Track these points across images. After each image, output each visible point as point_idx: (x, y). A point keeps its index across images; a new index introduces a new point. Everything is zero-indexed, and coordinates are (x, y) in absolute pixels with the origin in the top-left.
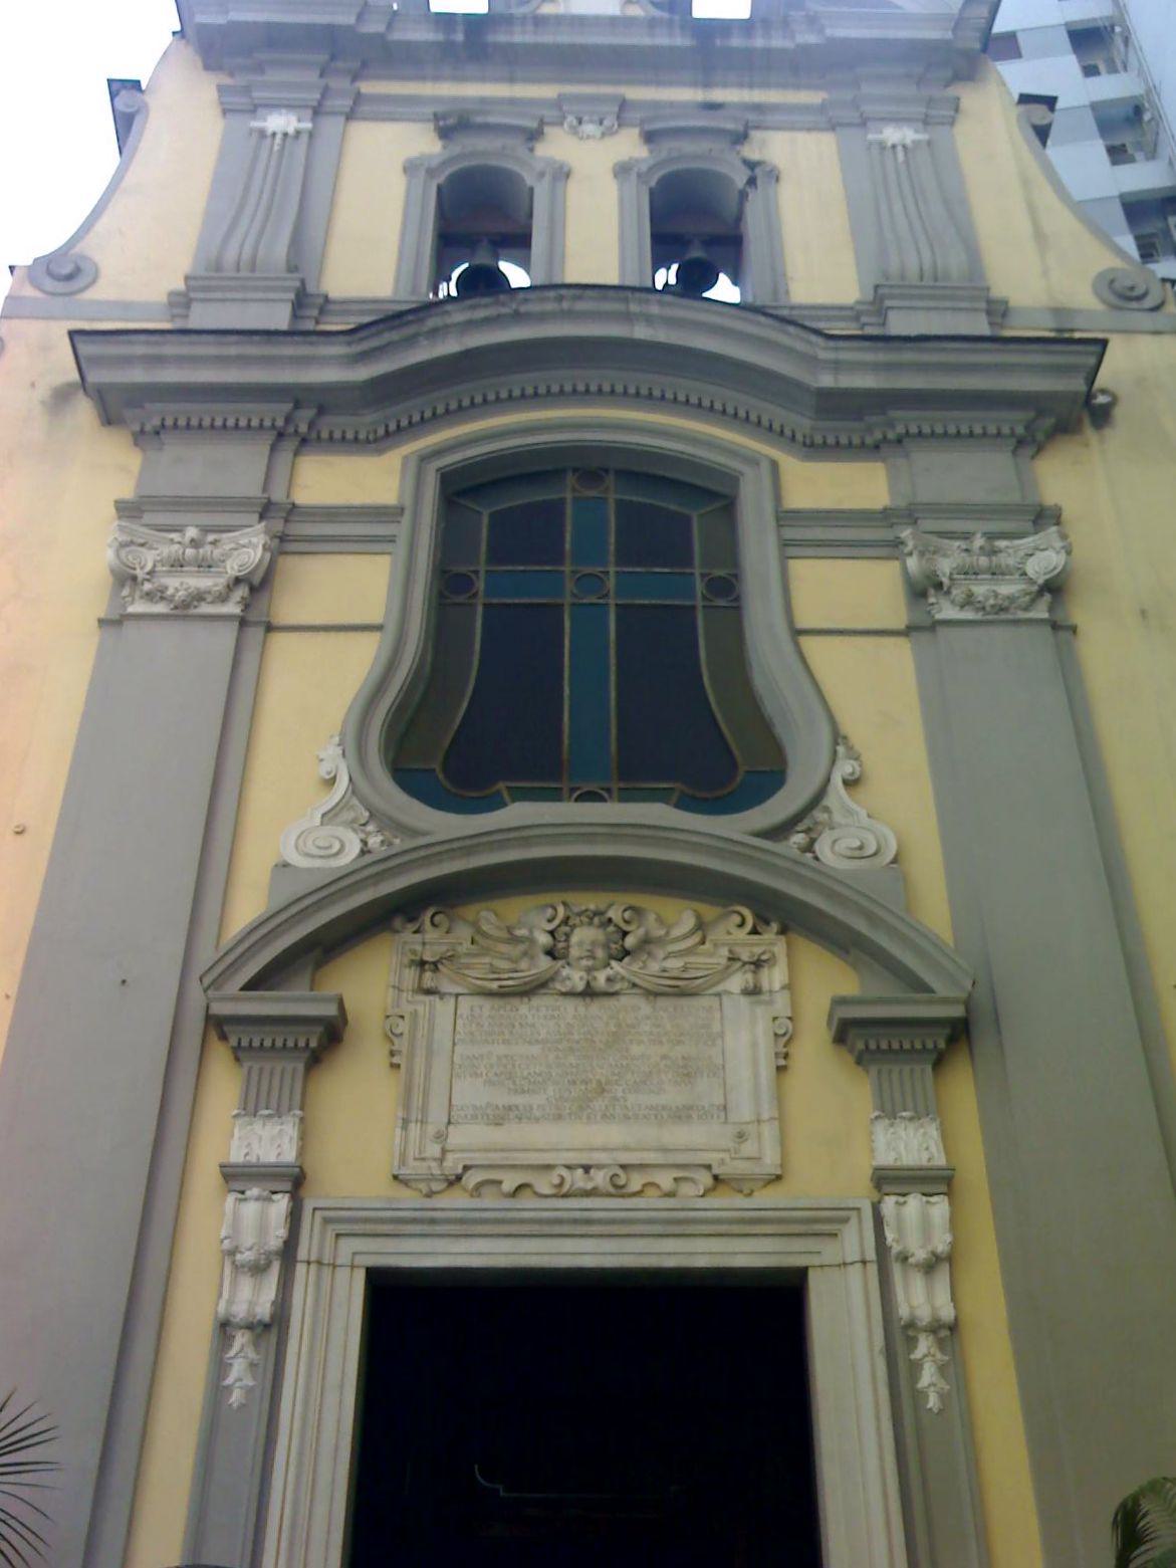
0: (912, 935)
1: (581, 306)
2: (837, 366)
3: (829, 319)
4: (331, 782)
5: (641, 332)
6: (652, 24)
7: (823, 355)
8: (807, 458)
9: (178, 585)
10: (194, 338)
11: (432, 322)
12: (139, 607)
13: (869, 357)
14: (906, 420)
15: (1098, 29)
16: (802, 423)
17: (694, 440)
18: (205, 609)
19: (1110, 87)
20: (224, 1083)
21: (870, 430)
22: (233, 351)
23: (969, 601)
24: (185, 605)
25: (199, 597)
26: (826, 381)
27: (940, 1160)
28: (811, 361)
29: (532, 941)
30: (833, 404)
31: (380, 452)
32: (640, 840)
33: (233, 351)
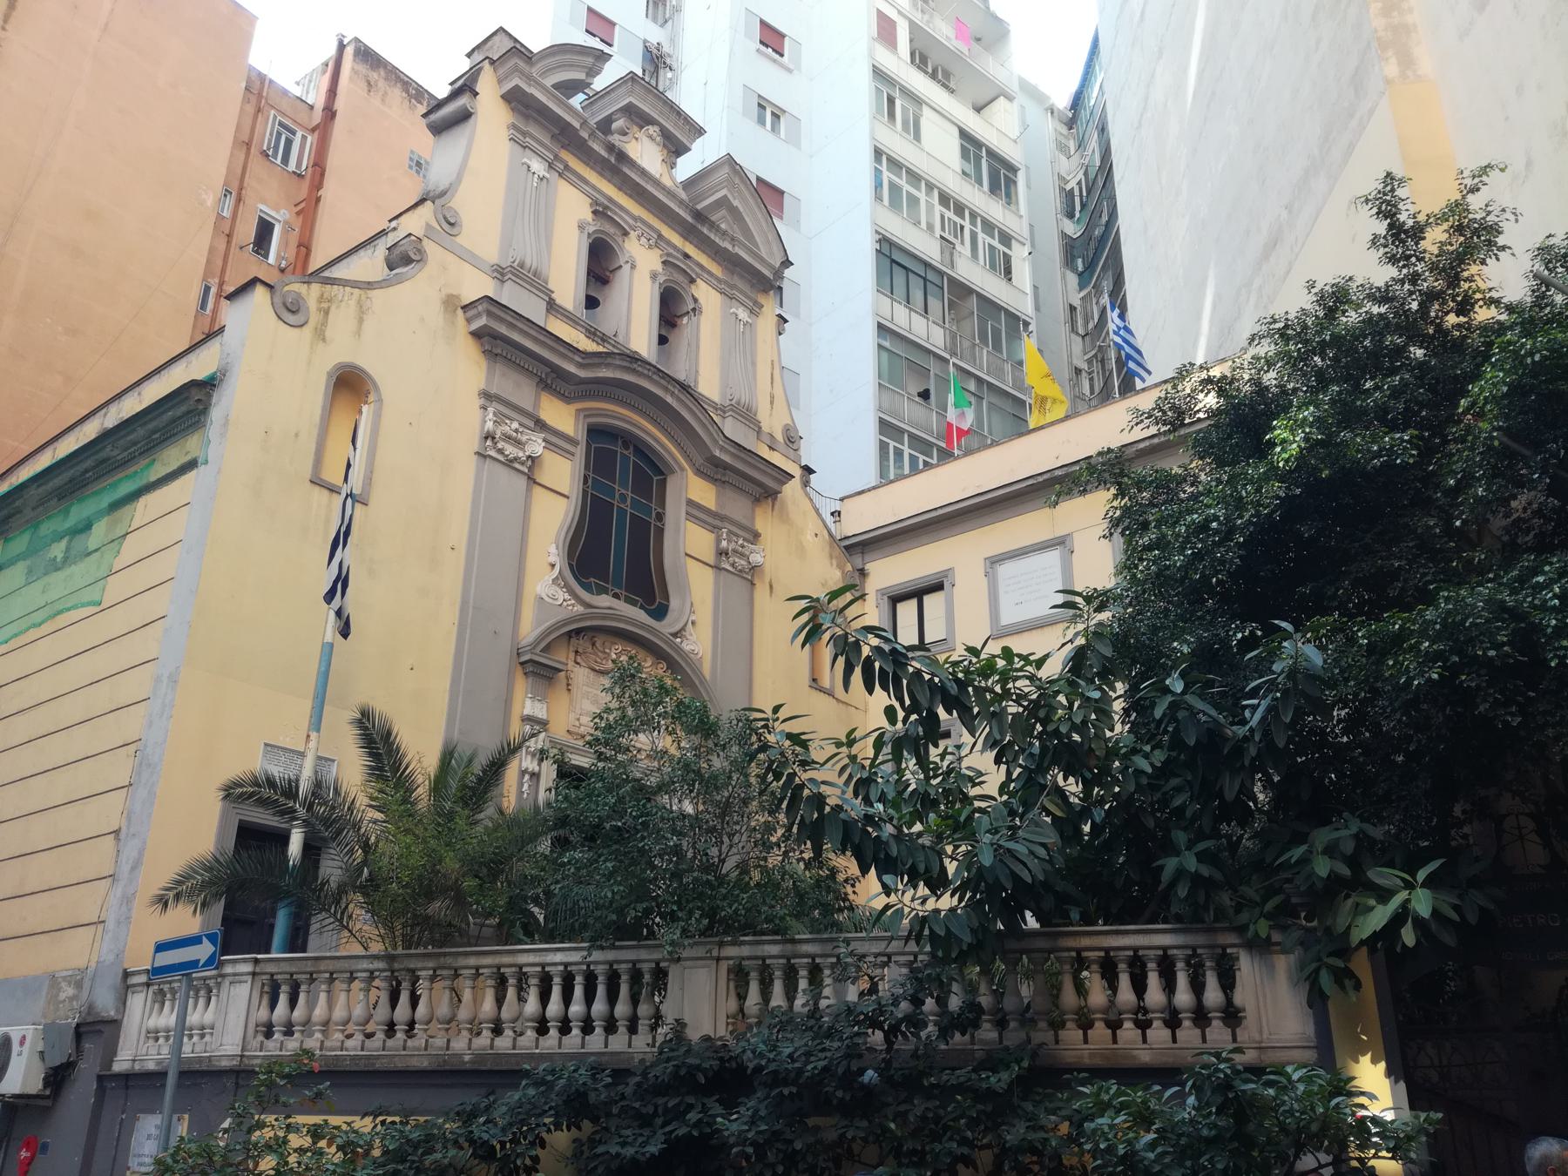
0: (161, 410)
1: (655, 377)
2: (722, 449)
3: (709, 405)
4: (553, 566)
5: (669, 399)
6: (681, 203)
7: (721, 443)
8: (696, 474)
9: (511, 450)
10: (530, 324)
11: (609, 360)
12: (493, 453)
13: (732, 450)
14: (730, 477)
15: (1180, 1069)
16: (699, 460)
17: (663, 446)
18: (517, 466)
19: (655, 34)
20: (521, 685)
21: (717, 473)
22: (542, 338)
23: (733, 565)
24: (511, 461)
25: (516, 459)
26: (717, 453)
27: (545, 717)
28: (716, 442)
29: (609, 654)
30: (717, 464)
31: (569, 404)
32: (650, 632)
33: (542, 338)
